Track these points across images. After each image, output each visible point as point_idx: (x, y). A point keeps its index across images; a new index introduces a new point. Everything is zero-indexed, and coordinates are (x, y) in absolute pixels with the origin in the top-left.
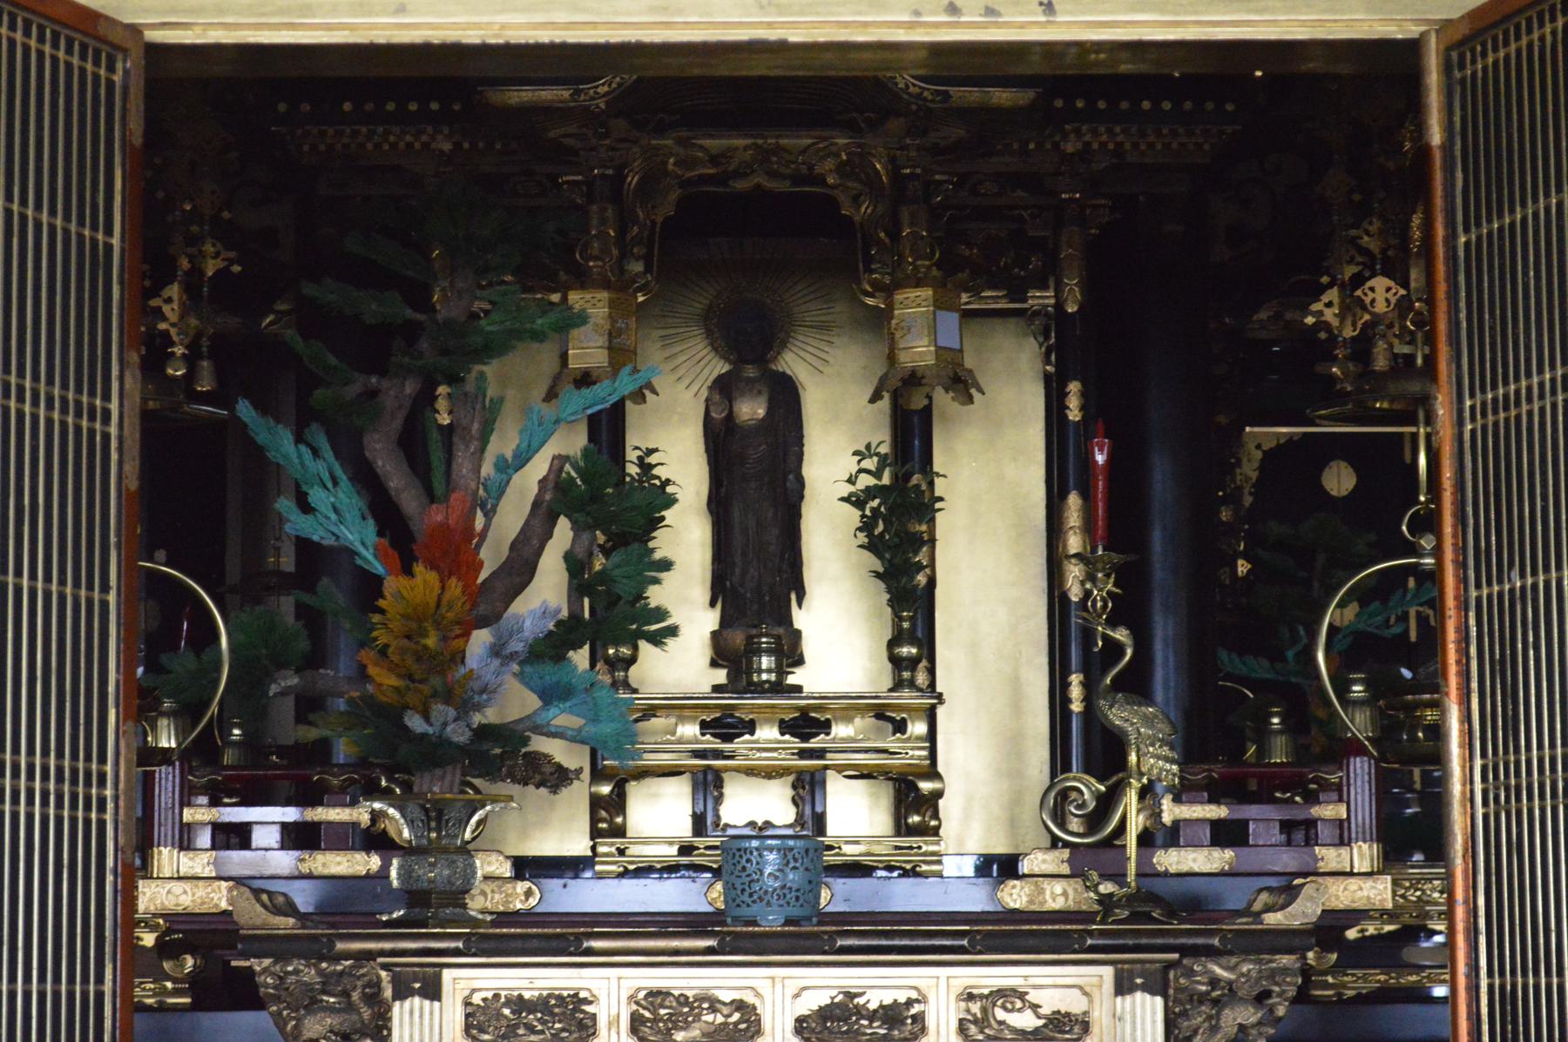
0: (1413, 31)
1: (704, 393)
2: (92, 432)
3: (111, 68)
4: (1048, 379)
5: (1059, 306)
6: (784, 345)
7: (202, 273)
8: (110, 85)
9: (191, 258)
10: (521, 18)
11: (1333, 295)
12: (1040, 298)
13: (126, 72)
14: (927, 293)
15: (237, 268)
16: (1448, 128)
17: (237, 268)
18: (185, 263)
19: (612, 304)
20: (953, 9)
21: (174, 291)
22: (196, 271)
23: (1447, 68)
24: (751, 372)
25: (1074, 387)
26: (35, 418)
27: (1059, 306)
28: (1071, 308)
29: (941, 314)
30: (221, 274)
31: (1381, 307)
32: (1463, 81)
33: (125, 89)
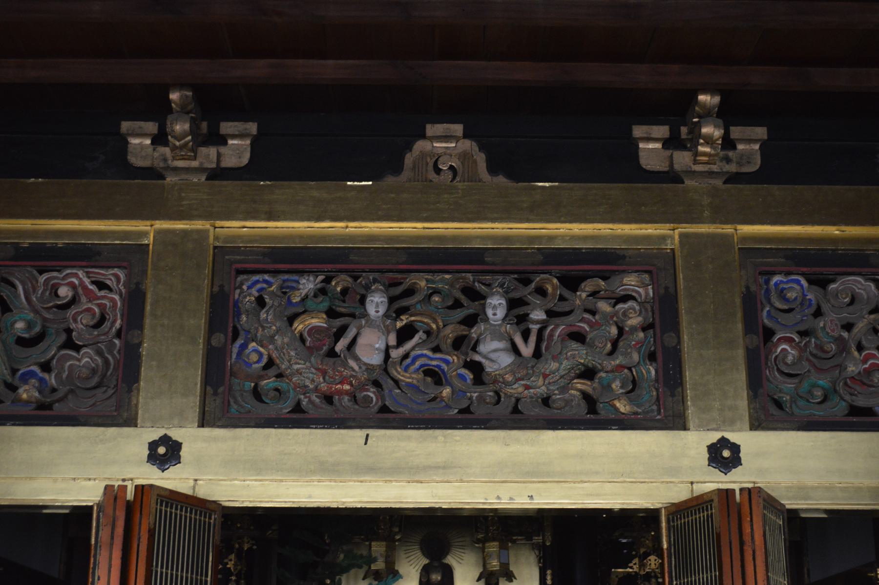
0: (658, 506)
1: (419, 571)
2: (205, 522)
3: (210, 518)
4: (540, 569)
5: (544, 542)
6: (447, 554)
7: (243, 549)
8: (210, 524)
9: (239, 544)
10: (352, 500)
11: (636, 560)
12: (538, 539)
13: (215, 519)
14: (496, 543)
15: (255, 547)
16: (669, 542)
17: (255, 547)
18: (237, 546)
19: (387, 547)
20: (498, 498)
21: (233, 556)
22: (241, 549)
23: (668, 521)
24: (436, 564)
25: (549, 572)
26: (186, 517)
27: (544, 542)
28: (548, 544)
29: (502, 551)
30: (250, 549)
31: (653, 566)
32: (674, 526)
33: (215, 524)
